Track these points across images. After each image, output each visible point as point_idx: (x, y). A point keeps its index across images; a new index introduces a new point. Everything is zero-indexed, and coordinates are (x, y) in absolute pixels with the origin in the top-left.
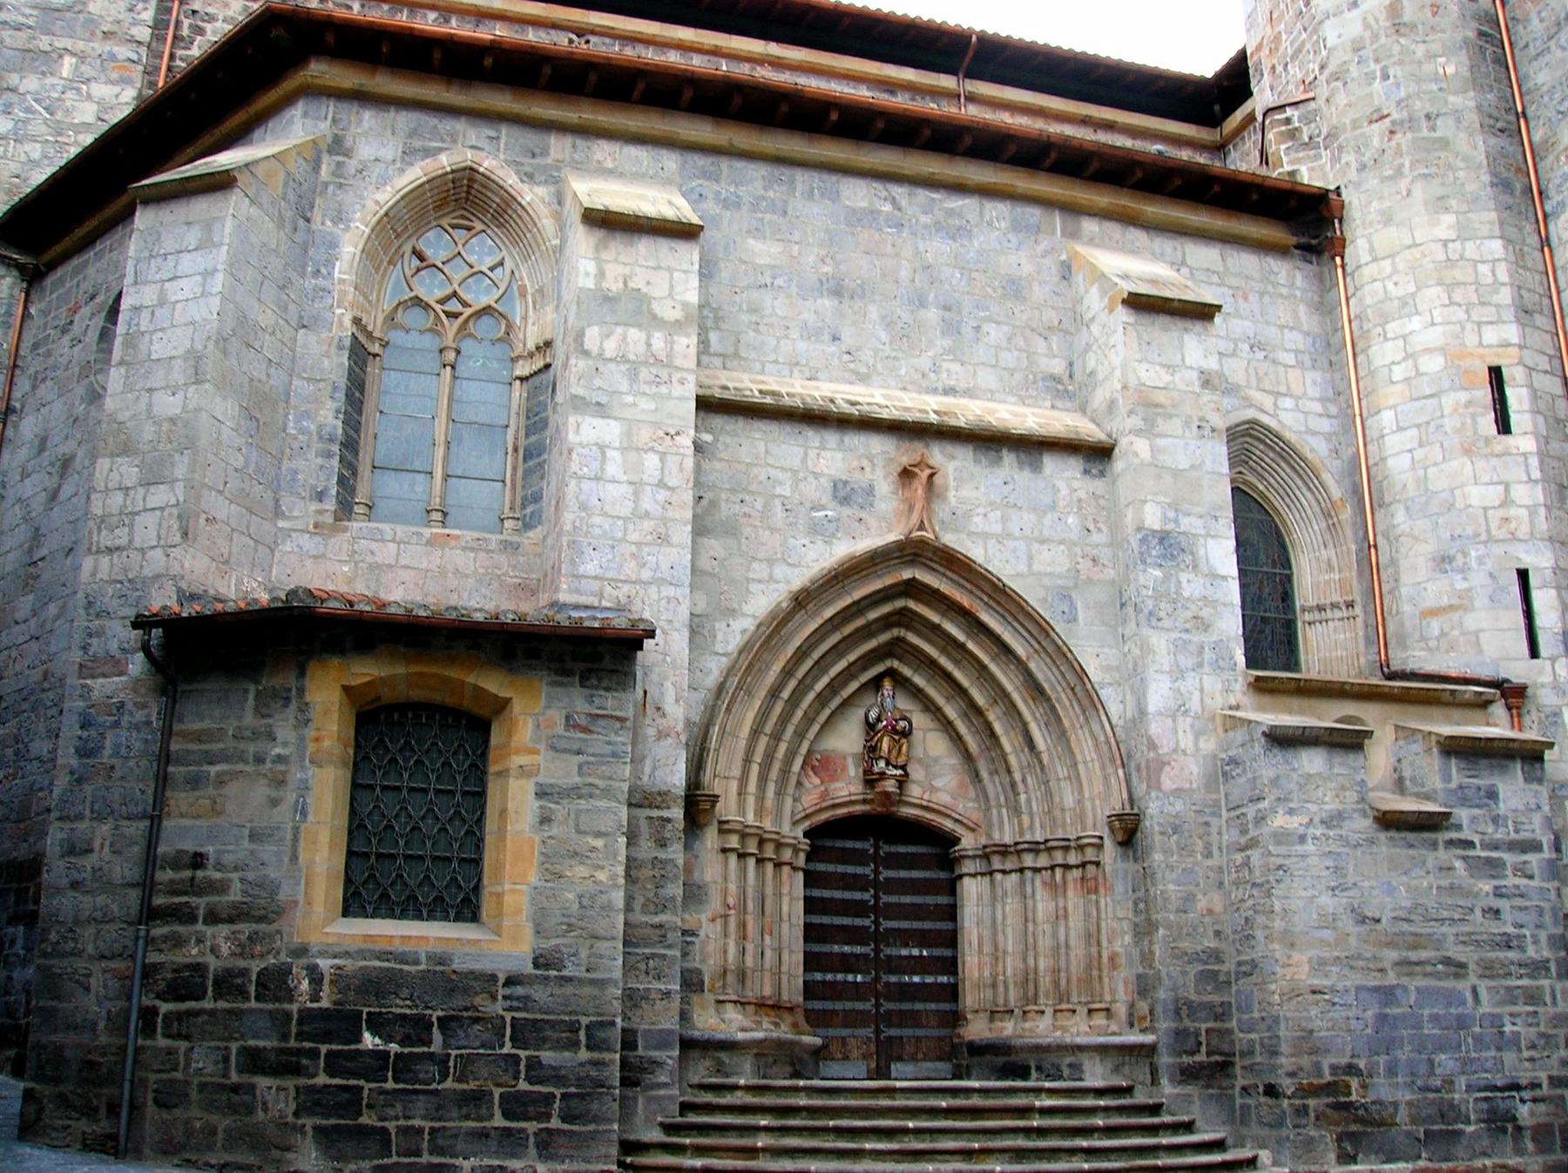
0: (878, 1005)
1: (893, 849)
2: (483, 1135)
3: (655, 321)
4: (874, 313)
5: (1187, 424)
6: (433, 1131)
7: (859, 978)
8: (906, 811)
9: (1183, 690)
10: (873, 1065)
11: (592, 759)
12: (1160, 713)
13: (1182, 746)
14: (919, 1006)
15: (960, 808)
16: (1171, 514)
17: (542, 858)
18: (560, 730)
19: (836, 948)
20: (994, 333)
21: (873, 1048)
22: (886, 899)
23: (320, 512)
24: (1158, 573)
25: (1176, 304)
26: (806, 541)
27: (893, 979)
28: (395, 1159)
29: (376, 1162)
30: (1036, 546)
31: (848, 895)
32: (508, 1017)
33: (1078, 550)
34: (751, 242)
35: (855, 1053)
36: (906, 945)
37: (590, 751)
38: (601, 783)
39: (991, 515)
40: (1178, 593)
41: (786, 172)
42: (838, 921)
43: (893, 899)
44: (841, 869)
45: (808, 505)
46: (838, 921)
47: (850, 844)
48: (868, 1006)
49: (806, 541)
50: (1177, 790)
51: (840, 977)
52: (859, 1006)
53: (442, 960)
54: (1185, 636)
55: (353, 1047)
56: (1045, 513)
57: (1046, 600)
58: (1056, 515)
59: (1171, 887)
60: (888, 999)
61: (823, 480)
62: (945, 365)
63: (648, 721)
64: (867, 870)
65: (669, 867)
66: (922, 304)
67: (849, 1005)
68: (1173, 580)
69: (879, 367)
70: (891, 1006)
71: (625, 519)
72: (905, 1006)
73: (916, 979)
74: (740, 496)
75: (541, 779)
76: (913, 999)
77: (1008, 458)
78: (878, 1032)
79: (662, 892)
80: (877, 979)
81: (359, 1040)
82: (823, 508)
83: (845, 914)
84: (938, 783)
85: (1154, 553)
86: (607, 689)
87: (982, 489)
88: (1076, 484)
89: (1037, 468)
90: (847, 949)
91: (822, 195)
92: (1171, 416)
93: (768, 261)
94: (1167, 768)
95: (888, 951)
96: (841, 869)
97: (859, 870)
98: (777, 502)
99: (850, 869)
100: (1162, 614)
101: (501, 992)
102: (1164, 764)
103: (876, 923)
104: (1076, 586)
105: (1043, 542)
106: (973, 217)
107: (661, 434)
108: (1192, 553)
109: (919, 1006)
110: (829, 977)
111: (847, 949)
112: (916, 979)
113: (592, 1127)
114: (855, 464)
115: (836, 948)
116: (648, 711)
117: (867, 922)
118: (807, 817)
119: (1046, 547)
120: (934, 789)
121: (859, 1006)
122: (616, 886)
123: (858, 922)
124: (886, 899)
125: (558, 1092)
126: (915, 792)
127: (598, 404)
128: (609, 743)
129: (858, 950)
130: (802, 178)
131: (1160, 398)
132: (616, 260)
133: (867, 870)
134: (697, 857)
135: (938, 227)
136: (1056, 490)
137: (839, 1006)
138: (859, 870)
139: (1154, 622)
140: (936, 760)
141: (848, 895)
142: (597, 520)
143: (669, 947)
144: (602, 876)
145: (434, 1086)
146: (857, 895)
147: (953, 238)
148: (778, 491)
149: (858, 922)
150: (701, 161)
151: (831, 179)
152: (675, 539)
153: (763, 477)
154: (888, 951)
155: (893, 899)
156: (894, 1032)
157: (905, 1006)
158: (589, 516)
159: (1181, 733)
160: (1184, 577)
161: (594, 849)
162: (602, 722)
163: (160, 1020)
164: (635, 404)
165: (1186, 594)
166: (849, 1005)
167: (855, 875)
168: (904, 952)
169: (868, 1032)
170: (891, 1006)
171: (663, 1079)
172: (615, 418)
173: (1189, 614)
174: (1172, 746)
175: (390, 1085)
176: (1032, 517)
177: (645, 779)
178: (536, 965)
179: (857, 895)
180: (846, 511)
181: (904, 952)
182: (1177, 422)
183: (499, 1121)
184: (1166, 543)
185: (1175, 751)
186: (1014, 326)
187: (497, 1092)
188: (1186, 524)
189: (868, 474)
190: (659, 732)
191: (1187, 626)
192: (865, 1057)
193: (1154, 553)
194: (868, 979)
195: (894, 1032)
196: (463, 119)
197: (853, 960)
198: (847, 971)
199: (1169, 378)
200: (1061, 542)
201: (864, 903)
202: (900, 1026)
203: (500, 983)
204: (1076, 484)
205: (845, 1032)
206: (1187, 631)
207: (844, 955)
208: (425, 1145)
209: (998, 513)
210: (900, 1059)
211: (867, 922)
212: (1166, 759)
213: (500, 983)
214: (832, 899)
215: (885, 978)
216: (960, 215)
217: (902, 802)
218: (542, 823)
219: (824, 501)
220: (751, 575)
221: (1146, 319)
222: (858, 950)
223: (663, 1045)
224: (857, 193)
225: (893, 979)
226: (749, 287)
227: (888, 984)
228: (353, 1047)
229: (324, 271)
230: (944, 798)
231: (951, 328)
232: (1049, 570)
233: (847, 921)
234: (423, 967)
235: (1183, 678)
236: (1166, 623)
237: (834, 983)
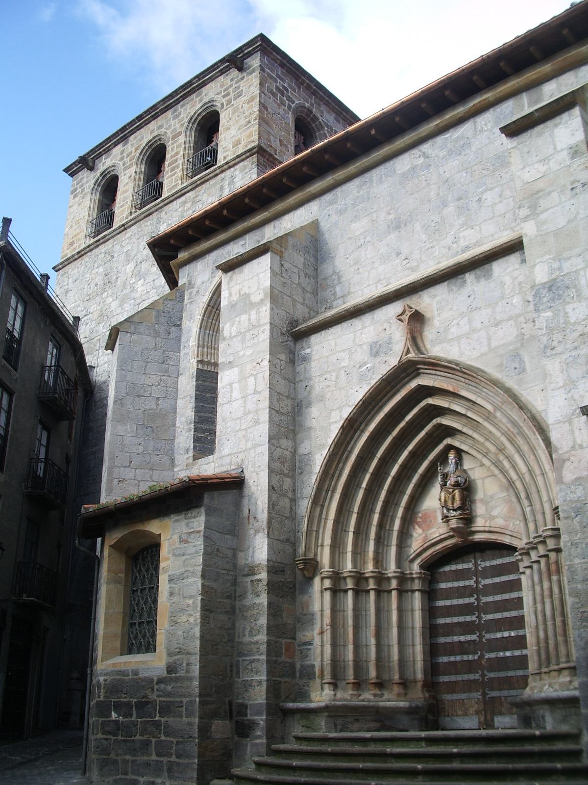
0: (483, 675)
1: (488, 564)
2: (147, 764)
3: (252, 305)
4: (418, 227)
5: (562, 192)
6: (133, 761)
7: (471, 657)
8: (478, 537)
9: (576, 397)
10: (482, 719)
11: (188, 557)
12: (559, 422)
13: (579, 442)
14: (511, 673)
15: (511, 527)
16: (556, 265)
17: (170, 614)
18: (177, 545)
19: (456, 639)
20: (490, 197)
21: (482, 707)
22: (485, 599)
23: (188, 459)
24: (549, 314)
25: (536, 115)
26: (357, 389)
27: (492, 655)
28: (120, 776)
29: (114, 777)
30: (493, 329)
31: (461, 601)
32: (158, 700)
33: (522, 319)
34: (353, 225)
35: (472, 710)
36: (500, 630)
37: (188, 552)
38: (191, 569)
39: (462, 323)
40: (566, 322)
41: (367, 175)
42: (456, 620)
43: (490, 599)
44: (456, 584)
45: (358, 366)
46: (456, 620)
47: (460, 567)
48: (476, 676)
49: (357, 389)
50: (577, 479)
51: (459, 658)
52: (472, 677)
53: (136, 673)
54: (574, 353)
55: (109, 719)
56: (497, 303)
57: (501, 365)
58: (504, 302)
59: (577, 561)
60: (490, 671)
61: (365, 347)
62: (461, 235)
63: (251, 526)
64: (471, 582)
65: (261, 607)
66: (445, 204)
67: (466, 677)
68: (562, 314)
69: (424, 258)
70: (492, 675)
71: (240, 418)
72: (502, 674)
73: (508, 654)
74: (324, 377)
75: (170, 573)
76: (508, 669)
77: (469, 277)
78: (484, 694)
79: (258, 622)
80: (481, 657)
81: (110, 715)
82: (365, 363)
83: (461, 614)
84: (495, 513)
85: (545, 300)
86: (194, 517)
87: (455, 308)
88: (516, 273)
89: (488, 276)
90: (462, 638)
91: (386, 177)
92: (549, 194)
93: (362, 230)
94: (568, 464)
95: (488, 636)
96: (456, 584)
97: (467, 583)
98: (342, 372)
99: (461, 584)
100: (555, 343)
101: (156, 687)
102: (564, 461)
103: (479, 617)
104: (522, 345)
105: (497, 325)
106: (470, 134)
107: (255, 364)
108: (575, 286)
109: (511, 673)
110: (452, 659)
111: (462, 638)
112: (508, 654)
113: (187, 761)
114: (381, 328)
115: (456, 639)
116: (251, 520)
117: (474, 618)
118: (418, 555)
119: (499, 327)
120: (493, 518)
121: (472, 677)
122: (196, 624)
123: (468, 619)
124: (485, 599)
125: (174, 741)
126: (480, 523)
127: (230, 362)
128: (194, 546)
129: (469, 638)
130: (375, 173)
131: (541, 185)
132: (236, 284)
133: (471, 582)
134: (310, 597)
135: (451, 152)
136: (502, 284)
137: (459, 678)
138: (467, 583)
139: (549, 352)
140: (492, 497)
141: (461, 601)
142: (229, 424)
143: (261, 654)
144: (192, 620)
145: (133, 738)
146: (467, 601)
147: (460, 154)
148: (343, 364)
149: (468, 619)
150: (328, 197)
151: (389, 165)
152: (261, 420)
153: (335, 360)
154: (488, 636)
155: (490, 599)
156: (495, 694)
157: (502, 674)
158: (226, 423)
159: (577, 432)
160: (569, 308)
161: (188, 606)
162: (192, 536)
163: (197, 714)
164: (244, 355)
165: (572, 320)
166: (466, 677)
167: (465, 587)
168: (499, 635)
169: (477, 695)
170: (492, 675)
171: (259, 733)
172: (236, 367)
173: (576, 334)
174: (571, 444)
175: (120, 738)
176: (489, 311)
177: (250, 559)
178: (168, 672)
179: (467, 601)
180: (378, 359)
181: (499, 635)
182: (555, 195)
183: (154, 757)
184: (554, 289)
185: (573, 448)
186: (502, 185)
187: (154, 740)
188: (567, 266)
189: (388, 332)
190: (256, 531)
191: (576, 344)
192: (477, 712)
193: (545, 300)
194: (476, 657)
195: (495, 694)
196: (232, 243)
197: (466, 645)
198: (463, 653)
199: (545, 168)
200: (509, 319)
201: (470, 605)
202: (500, 689)
203: (155, 683)
204: (516, 273)
205: (463, 696)
206: (576, 348)
207: (461, 643)
208: (130, 769)
209: (466, 319)
210: (501, 713)
211: (474, 618)
212: (566, 457)
213: (155, 683)
214: (451, 606)
215: (487, 656)
216: (462, 138)
217: (474, 532)
218: (170, 595)
219: (365, 360)
220: (331, 421)
221: (525, 137)
222: (469, 638)
223: (258, 713)
224: (403, 163)
225: (492, 655)
226: (353, 251)
227: (489, 659)
228: (109, 719)
229: (186, 345)
230: (499, 522)
231: (462, 210)
232: (502, 342)
233: (461, 619)
234: (130, 677)
235: (575, 387)
236: (559, 349)
237: (455, 663)
